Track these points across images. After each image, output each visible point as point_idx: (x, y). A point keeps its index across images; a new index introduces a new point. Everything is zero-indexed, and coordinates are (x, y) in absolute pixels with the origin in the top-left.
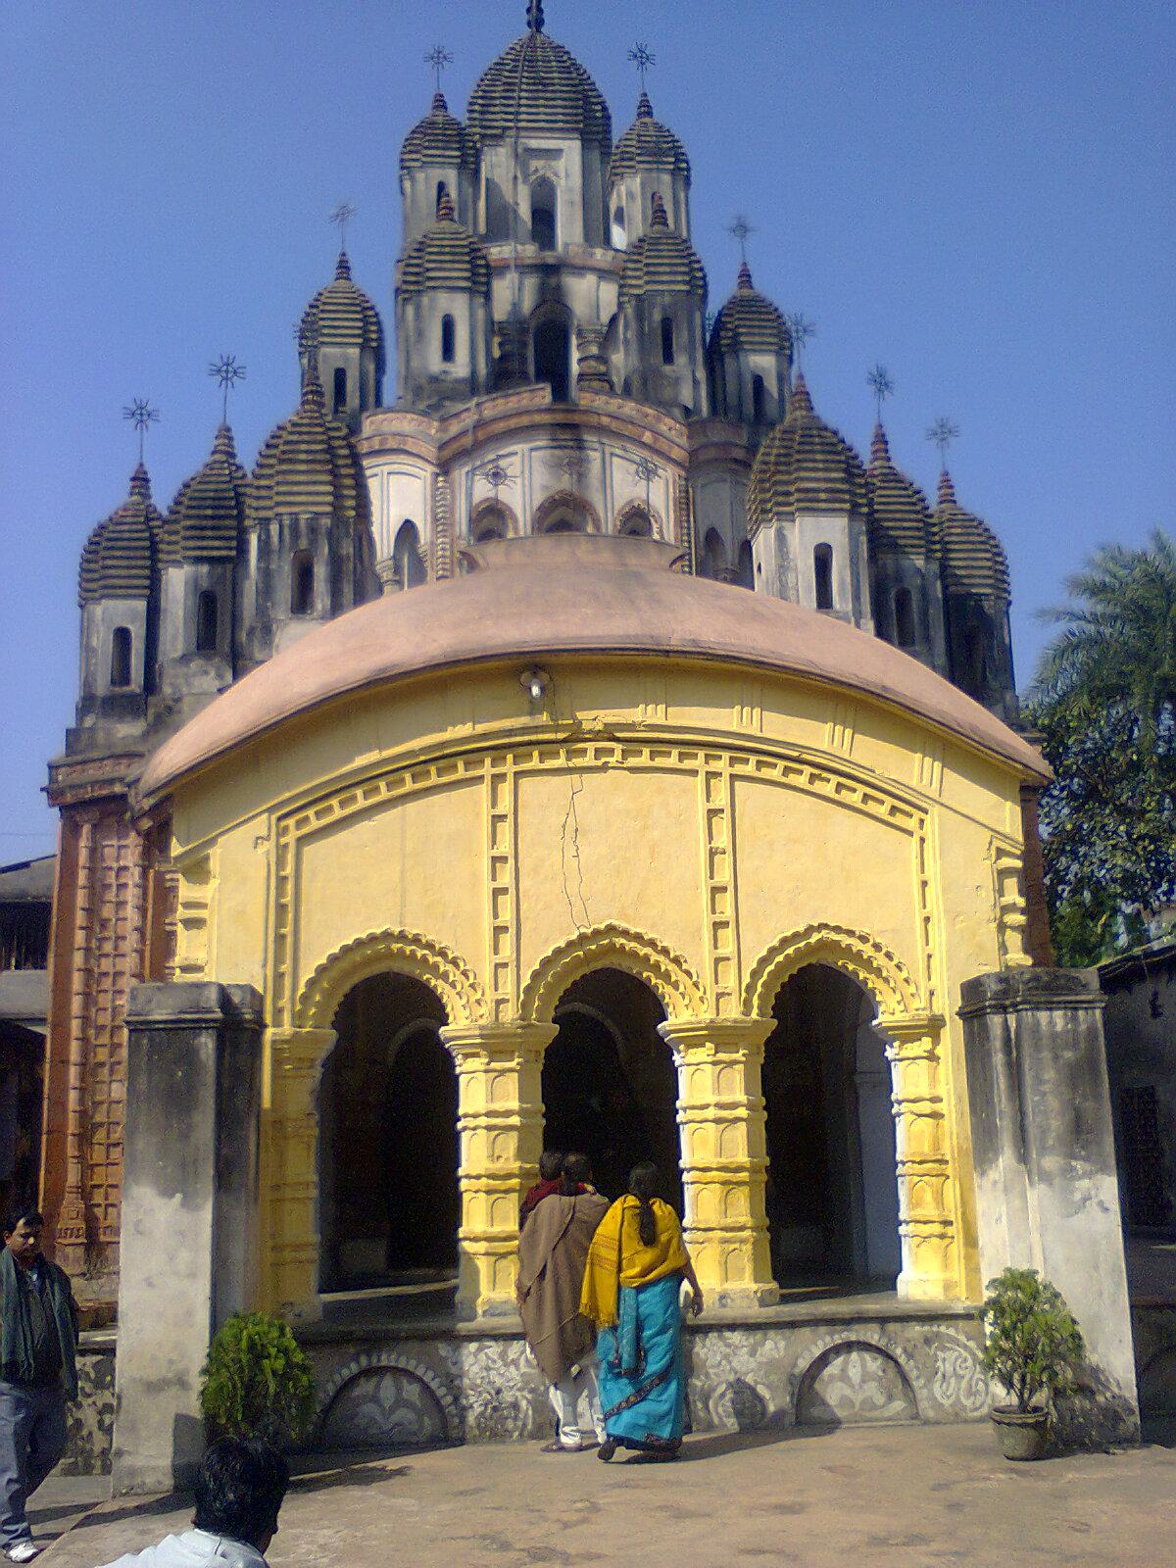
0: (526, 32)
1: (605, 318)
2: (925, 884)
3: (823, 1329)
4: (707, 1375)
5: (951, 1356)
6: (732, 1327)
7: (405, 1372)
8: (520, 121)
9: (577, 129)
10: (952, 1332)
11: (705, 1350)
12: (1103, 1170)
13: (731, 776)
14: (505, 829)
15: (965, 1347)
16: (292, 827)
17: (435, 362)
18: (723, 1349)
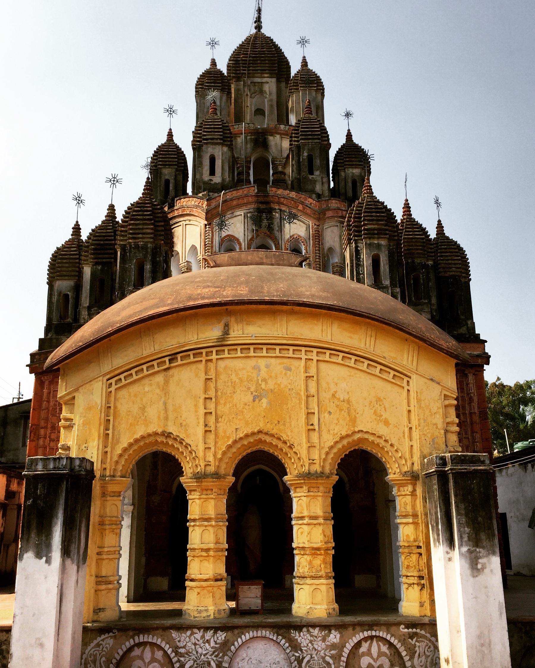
0: (254, 31)
1: (285, 155)
2: (409, 411)
3: (358, 628)
4: (301, 650)
5: (424, 644)
6: (314, 626)
7: (155, 644)
8: (250, 70)
9: (275, 73)
10: (423, 632)
11: (301, 638)
12: (494, 553)
13: (317, 361)
14: (212, 385)
15: (430, 640)
16: (113, 384)
17: (206, 177)
18: (309, 638)
